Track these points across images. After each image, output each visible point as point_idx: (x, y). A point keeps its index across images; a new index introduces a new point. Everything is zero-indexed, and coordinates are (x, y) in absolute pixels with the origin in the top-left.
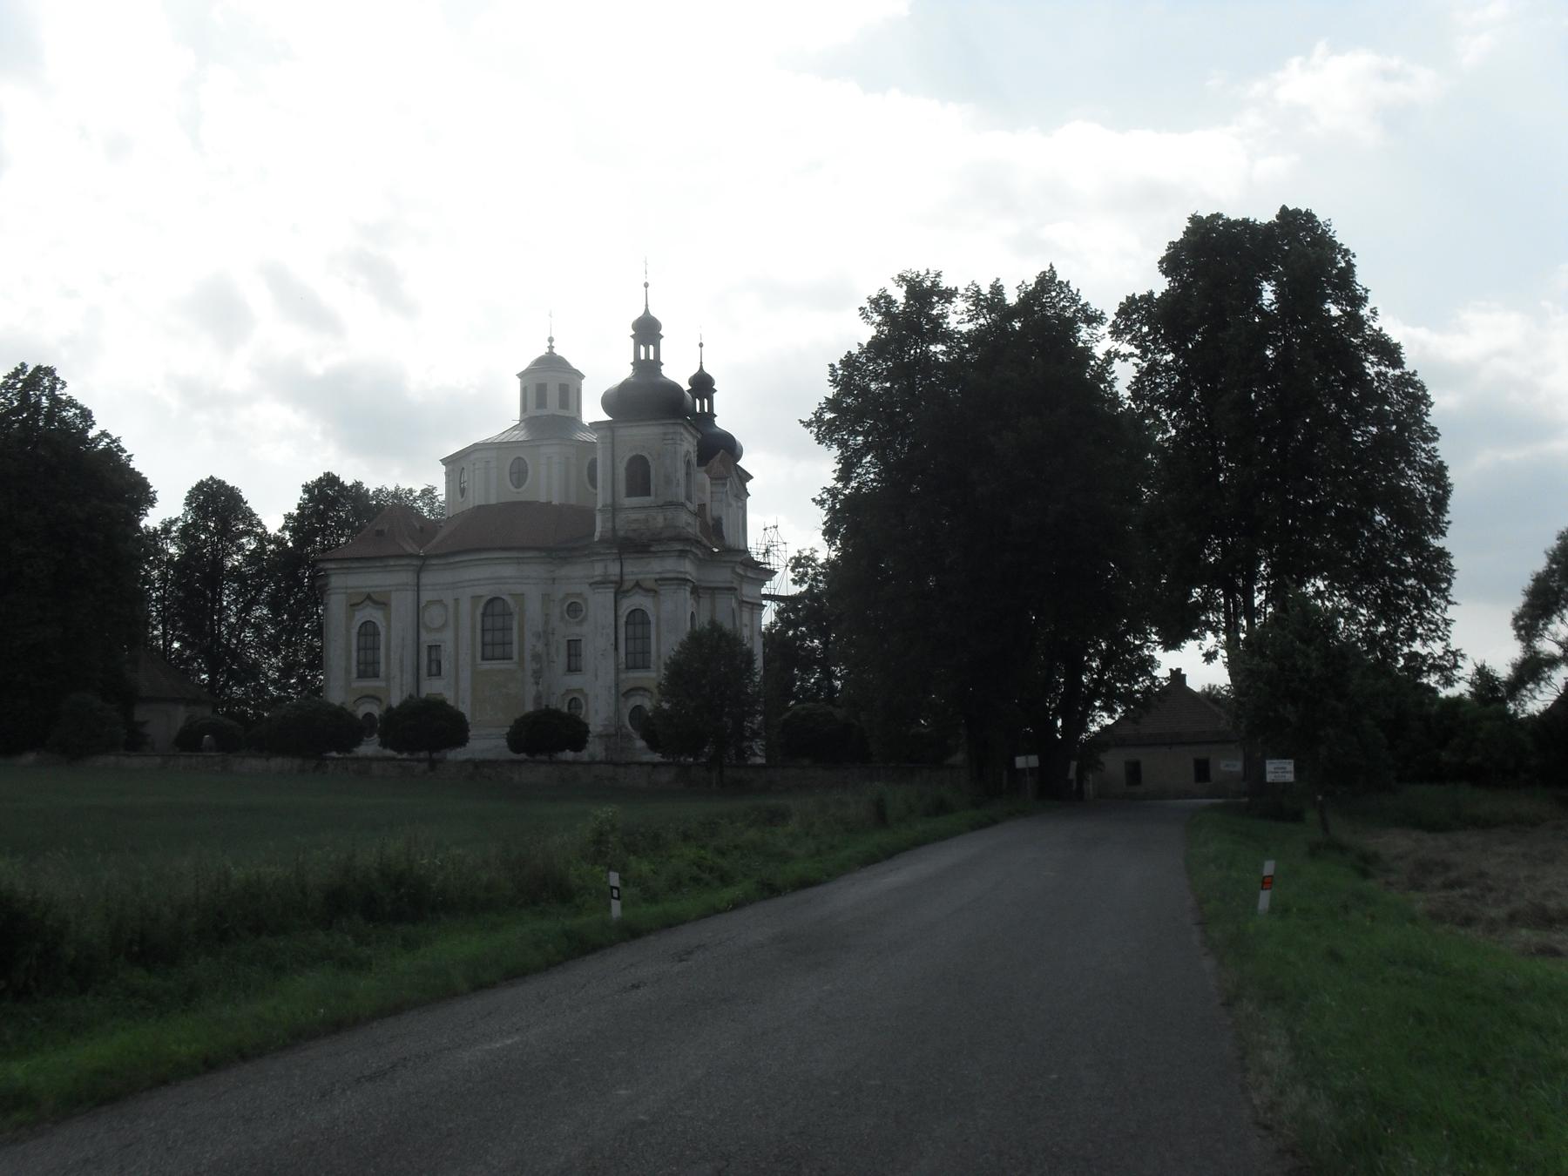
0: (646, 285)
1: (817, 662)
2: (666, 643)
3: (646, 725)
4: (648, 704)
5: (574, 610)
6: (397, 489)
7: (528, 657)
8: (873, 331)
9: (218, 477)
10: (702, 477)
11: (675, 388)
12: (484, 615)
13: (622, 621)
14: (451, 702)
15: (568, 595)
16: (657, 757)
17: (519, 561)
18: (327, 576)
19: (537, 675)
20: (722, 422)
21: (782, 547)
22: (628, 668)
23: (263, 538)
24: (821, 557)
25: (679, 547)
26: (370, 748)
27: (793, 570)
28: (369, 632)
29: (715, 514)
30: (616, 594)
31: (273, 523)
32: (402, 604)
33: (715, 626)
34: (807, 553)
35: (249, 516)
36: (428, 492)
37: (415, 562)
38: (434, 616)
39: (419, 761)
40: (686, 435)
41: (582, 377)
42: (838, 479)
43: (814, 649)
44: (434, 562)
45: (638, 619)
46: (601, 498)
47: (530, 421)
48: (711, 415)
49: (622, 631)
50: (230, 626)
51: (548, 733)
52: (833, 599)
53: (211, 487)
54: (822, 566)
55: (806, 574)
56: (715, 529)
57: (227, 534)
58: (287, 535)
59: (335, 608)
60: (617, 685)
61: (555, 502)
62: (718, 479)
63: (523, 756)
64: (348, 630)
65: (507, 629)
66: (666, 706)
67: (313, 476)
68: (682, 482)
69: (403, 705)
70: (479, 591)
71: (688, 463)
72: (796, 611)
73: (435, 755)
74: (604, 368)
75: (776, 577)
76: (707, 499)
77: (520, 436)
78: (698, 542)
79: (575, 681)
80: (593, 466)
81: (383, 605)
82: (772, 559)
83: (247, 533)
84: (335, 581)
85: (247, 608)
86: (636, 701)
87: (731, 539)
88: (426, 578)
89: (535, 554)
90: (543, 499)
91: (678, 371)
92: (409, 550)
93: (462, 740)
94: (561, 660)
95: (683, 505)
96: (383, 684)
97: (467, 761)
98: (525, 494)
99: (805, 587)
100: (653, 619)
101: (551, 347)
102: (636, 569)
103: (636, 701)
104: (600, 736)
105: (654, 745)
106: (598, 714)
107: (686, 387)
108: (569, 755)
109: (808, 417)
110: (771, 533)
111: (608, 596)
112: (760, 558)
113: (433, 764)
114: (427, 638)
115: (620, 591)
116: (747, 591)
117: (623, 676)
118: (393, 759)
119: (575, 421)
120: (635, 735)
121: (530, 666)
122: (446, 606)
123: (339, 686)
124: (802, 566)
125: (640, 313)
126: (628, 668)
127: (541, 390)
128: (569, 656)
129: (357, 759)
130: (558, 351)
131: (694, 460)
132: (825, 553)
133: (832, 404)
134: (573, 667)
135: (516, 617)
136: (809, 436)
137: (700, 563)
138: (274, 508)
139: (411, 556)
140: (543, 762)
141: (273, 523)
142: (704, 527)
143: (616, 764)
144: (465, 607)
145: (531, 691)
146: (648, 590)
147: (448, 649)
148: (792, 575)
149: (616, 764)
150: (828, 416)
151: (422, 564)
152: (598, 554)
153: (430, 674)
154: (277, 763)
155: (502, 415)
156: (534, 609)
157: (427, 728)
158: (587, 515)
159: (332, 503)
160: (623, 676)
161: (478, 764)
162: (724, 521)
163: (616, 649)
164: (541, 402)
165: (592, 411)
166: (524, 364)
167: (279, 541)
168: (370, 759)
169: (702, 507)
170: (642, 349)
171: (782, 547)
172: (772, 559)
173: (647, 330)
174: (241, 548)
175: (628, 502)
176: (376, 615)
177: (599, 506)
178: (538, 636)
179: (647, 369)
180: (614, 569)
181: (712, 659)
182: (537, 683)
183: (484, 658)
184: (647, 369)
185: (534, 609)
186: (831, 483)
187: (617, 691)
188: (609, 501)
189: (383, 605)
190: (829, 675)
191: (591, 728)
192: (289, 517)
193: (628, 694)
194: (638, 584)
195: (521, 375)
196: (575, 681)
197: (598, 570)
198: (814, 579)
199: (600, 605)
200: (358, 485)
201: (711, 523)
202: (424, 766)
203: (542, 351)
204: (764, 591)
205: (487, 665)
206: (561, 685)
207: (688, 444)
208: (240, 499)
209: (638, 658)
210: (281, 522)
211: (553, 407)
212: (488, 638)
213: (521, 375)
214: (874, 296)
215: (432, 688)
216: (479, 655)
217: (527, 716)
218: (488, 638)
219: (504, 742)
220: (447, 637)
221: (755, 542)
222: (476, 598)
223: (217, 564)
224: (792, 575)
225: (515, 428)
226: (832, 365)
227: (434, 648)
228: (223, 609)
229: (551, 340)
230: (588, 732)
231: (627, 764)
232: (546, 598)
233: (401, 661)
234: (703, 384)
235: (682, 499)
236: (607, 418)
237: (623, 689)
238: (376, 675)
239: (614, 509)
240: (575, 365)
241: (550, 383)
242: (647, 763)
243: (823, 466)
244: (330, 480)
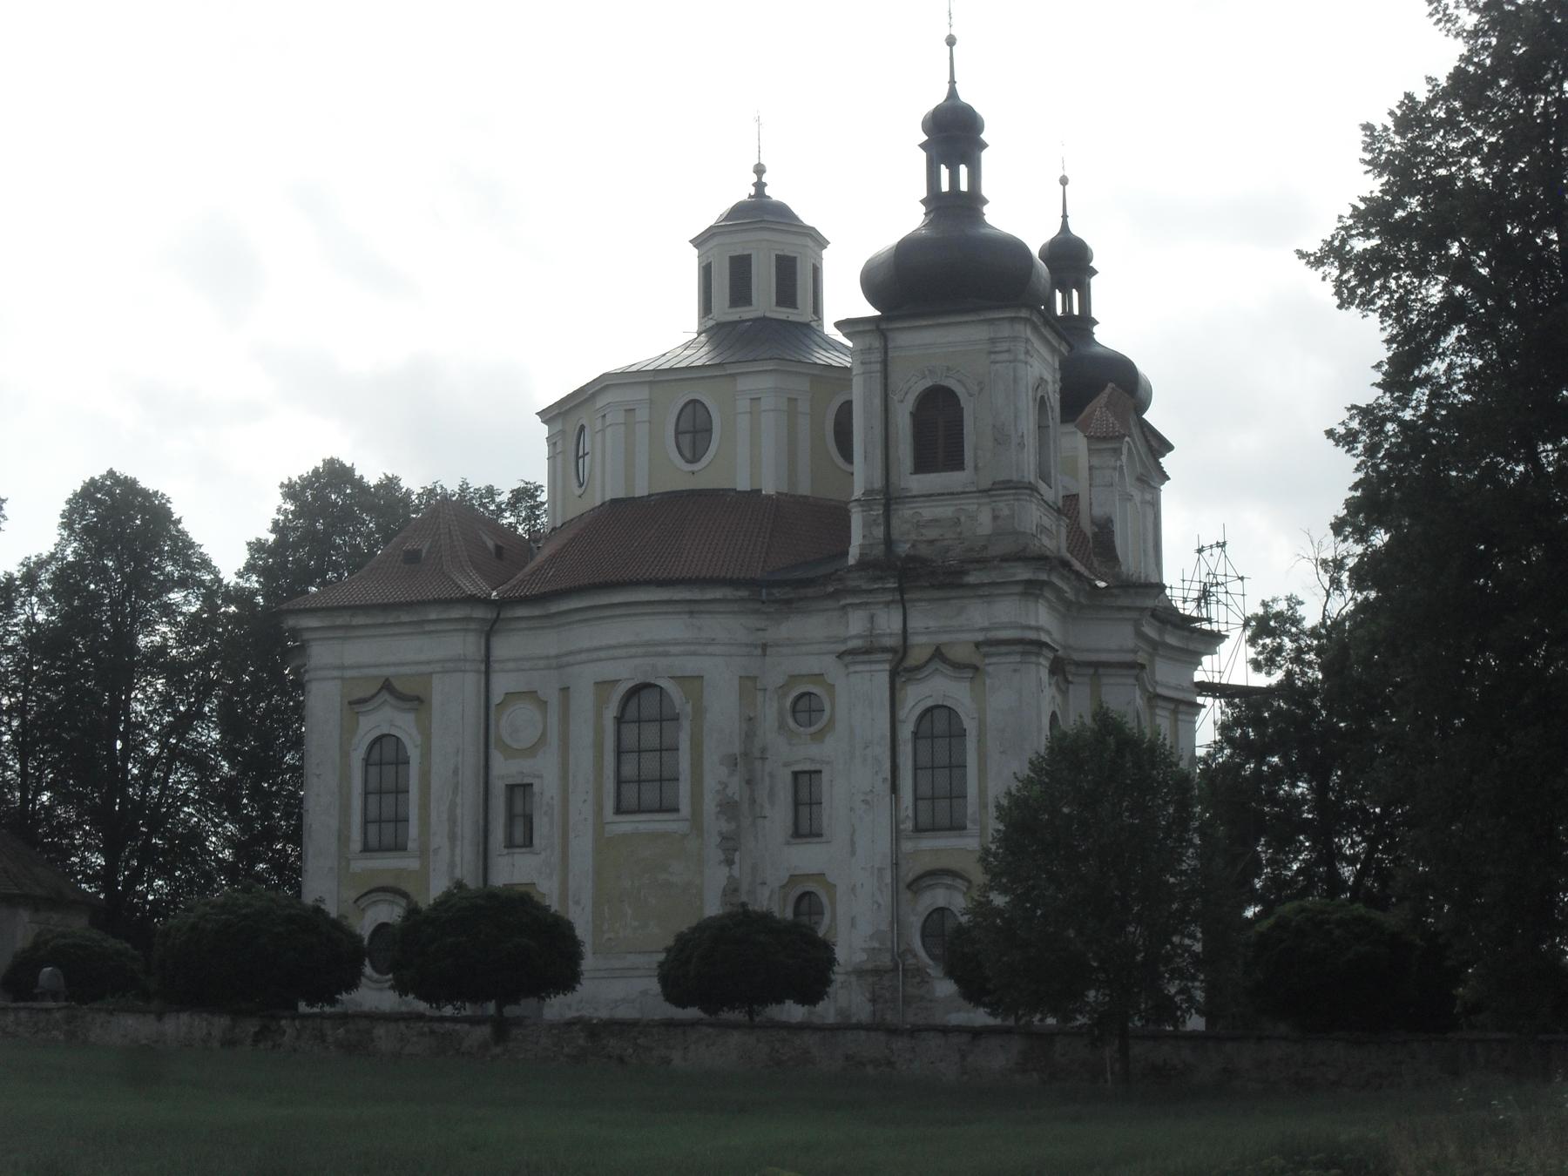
0: (951, 41)
1: (1305, 827)
2: (997, 772)
3: (959, 950)
4: (958, 902)
5: (806, 708)
6: (464, 488)
7: (710, 804)
8: (1460, 47)
9: (125, 470)
10: (1074, 443)
11: (1015, 249)
12: (619, 720)
13: (906, 732)
14: (662, 957)
15: (794, 678)
16: (980, 1017)
17: (692, 609)
18: (302, 649)
19: (730, 845)
20: (1109, 335)
21: (1234, 587)
22: (918, 829)
23: (214, 593)
24: (1311, 617)
25: (1023, 573)
26: (373, 994)
27: (1252, 641)
28: (386, 756)
29: (1098, 512)
30: (894, 675)
31: (228, 558)
32: (455, 700)
33: (1106, 723)
34: (1282, 606)
35: (183, 548)
36: (524, 495)
37: (479, 613)
38: (519, 723)
39: (474, 1021)
40: (1037, 344)
41: (822, 243)
42: (1385, 386)
43: (1298, 802)
44: (521, 612)
45: (940, 728)
46: (862, 475)
47: (716, 331)
48: (1084, 323)
49: (906, 751)
50: (149, 763)
51: (749, 963)
52: (1335, 703)
53: (110, 493)
54: (1314, 633)
55: (1279, 650)
56: (1101, 544)
57: (143, 588)
58: (254, 582)
59: (322, 703)
60: (896, 865)
61: (769, 489)
62: (1103, 440)
63: (693, 1013)
64: (345, 754)
65: (667, 749)
66: (999, 900)
67: (303, 465)
68: (1031, 442)
69: (441, 904)
70: (608, 671)
71: (1042, 403)
72: (1258, 723)
73: (511, 1011)
74: (863, 214)
75: (1224, 648)
76: (1081, 487)
77: (700, 356)
78: (1066, 564)
79: (806, 857)
80: (846, 410)
81: (415, 701)
82: (1215, 611)
83: (182, 583)
84: (321, 654)
85: (182, 725)
86: (938, 897)
87: (1130, 563)
88: (504, 648)
89: (728, 592)
90: (743, 484)
91: (1018, 211)
92: (470, 589)
93: (567, 978)
94: (779, 816)
95: (1032, 488)
96: (413, 864)
97: (570, 1024)
98: (706, 475)
99: (1278, 676)
100: (970, 725)
101: (760, 186)
102: (930, 623)
103: (938, 897)
104: (860, 973)
105: (973, 992)
106: (857, 928)
107: (1035, 250)
108: (794, 1012)
109: (1314, 246)
110: (1213, 559)
111: (876, 679)
112: (1189, 609)
113: (502, 1028)
114: (505, 770)
115: (902, 670)
116: (1165, 674)
117: (907, 846)
118: (420, 1017)
119: (808, 331)
120: (935, 971)
121: (715, 825)
122: (543, 705)
123: (334, 876)
124: (1272, 633)
125: (939, 97)
126: (918, 829)
127: (740, 269)
128: (797, 804)
129: (345, 1018)
130: (774, 192)
131: (1054, 400)
132: (1321, 603)
133: (1372, 215)
134: (805, 829)
135: (686, 724)
136: (1320, 286)
137: (1069, 611)
138: (227, 526)
139: (472, 600)
140: (736, 1026)
141: (228, 558)
142: (1075, 531)
143: (893, 1031)
144: (584, 700)
145: (715, 879)
146: (958, 666)
147: (547, 787)
148: (1251, 653)
149: (893, 1031)
150: (1359, 245)
151: (494, 618)
152: (855, 591)
153: (510, 844)
154: (179, 1026)
155: (663, 321)
156: (722, 708)
157: (494, 951)
158: (834, 517)
159: (342, 518)
160: (907, 846)
161: (596, 1030)
162: (1117, 528)
163: (894, 788)
164: (741, 292)
165: (843, 298)
166: (710, 213)
167: (240, 596)
168: (375, 1017)
169: (1072, 499)
170: (945, 172)
171: (1234, 587)
172: (1215, 611)
173: (953, 134)
174: (169, 611)
175: (918, 483)
176: (403, 724)
177: (858, 493)
178: (732, 762)
179: (954, 209)
180: (889, 622)
181: (1105, 783)
182: (730, 862)
183: (619, 810)
184: (954, 209)
185: (722, 708)
186: (1368, 394)
187: (896, 879)
188: (878, 484)
189: (415, 701)
190: (1330, 856)
191: (841, 953)
192: (257, 547)
193: (917, 884)
194: (938, 654)
195: (698, 242)
196: (806, 857)
197: (856, 624)
198: (1297, 658)
199: (861, 700)
200: (390, 484)
201: (1088, 528)
202: (484, 1032)
203: (743, 191)
204: (1199, 676)
205: (627, 825)
206: (776, 866)
207: (1040, 366)
208: (168, 513)
209: (939, 808)
210: (242, 557)
211: (764, 302)
212: (629, 770)
213: (698, 242)
214: (1337, 301)
215: (512, 870)
216: (609, 804)
217: (704, 927)
218: (629, 770)
219: (654, 986)
220: (544, 773)
221: (1179, 576)
222: (604, 686)
223: (124, 639)
224: (1251, 653)
225: (687, 346)
226: (1368, 128)
227: (519, 791)
228: (133, 727)
229: (759, 170)
230: (831, 961)
231: (915, 1031)
232: (749, 685)
233: (452, 820)
234: (1070, 260)
235: (1031, 476)
236: (870, 311)
237: (910, 871)
238: (399, 847)
239: (888, 498)
240: (807, 217)
241: (756, 259)
242: (959, 1029)
243: (1349, 352)
244: (336, 474)
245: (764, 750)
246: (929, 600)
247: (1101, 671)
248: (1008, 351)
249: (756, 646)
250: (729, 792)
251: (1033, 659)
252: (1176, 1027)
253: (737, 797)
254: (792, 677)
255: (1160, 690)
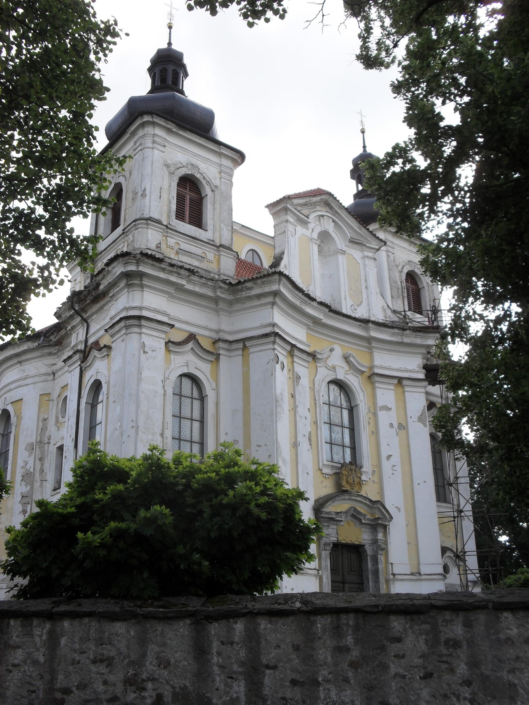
178: (31, 448)
245: (49, 438)
246: (96, 312)
247: (248, 344)
248: (140, 144)
249: (48, 374)
250: (28, 467)
251: (136, 330)
252: (273, 592)
253: (32, 470)
254: (62, 388)
255: (377, 371)
